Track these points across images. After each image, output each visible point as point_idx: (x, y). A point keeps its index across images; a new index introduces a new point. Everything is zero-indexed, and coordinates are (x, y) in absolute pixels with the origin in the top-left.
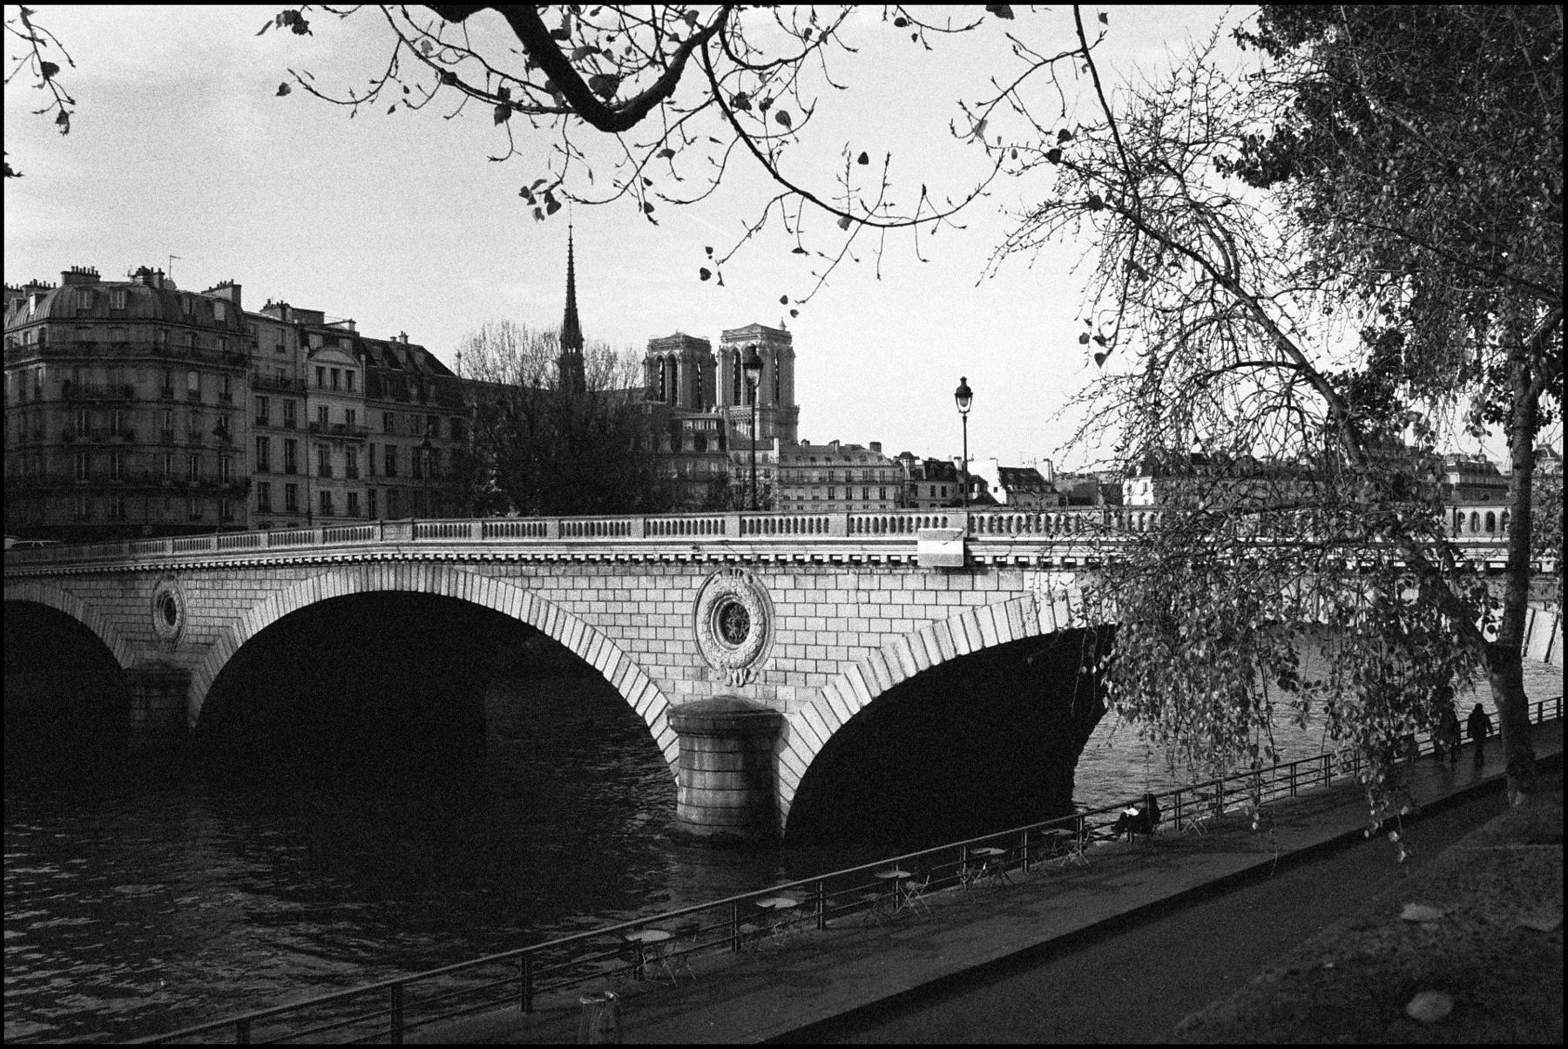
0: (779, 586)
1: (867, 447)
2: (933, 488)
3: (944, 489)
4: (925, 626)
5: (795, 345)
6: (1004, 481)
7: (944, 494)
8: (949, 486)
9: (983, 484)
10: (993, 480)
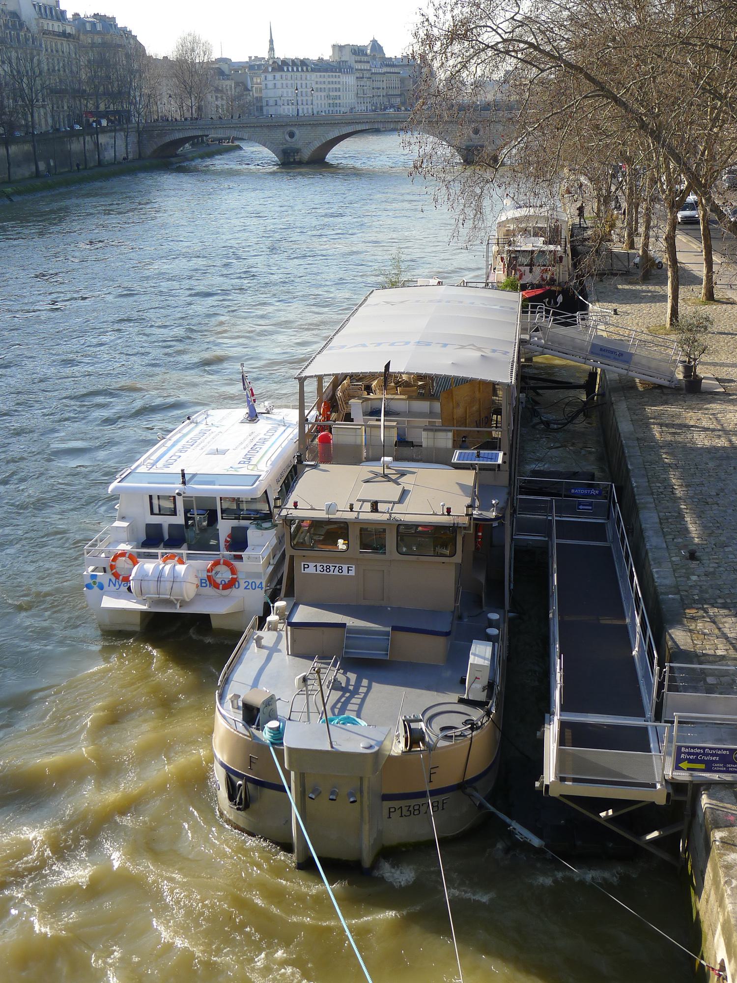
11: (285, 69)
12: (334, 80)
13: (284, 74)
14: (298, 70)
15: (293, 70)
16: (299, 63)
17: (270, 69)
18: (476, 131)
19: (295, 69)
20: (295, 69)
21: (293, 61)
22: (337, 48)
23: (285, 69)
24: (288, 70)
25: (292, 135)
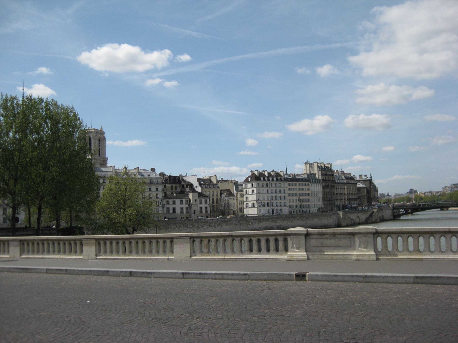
1: (150, 170)
2: (253, 184)
3: (176, 187)
5: (106, 135)
6: (200, 185)
7: (176, 189)
8: (178, 185)
9: (191, 185)
10: (196, 183)
11: (262, 179)
12: (294, 187)
13: (261, 183)
14: (273, 180)
15: (268, 180)
16: (266, 174)
17: (250, 179)
19: (271, 179)
20: (271, 179)
21: (269, 174)
22: (308, 165)
23: (262, 179)
24: (264, 180)
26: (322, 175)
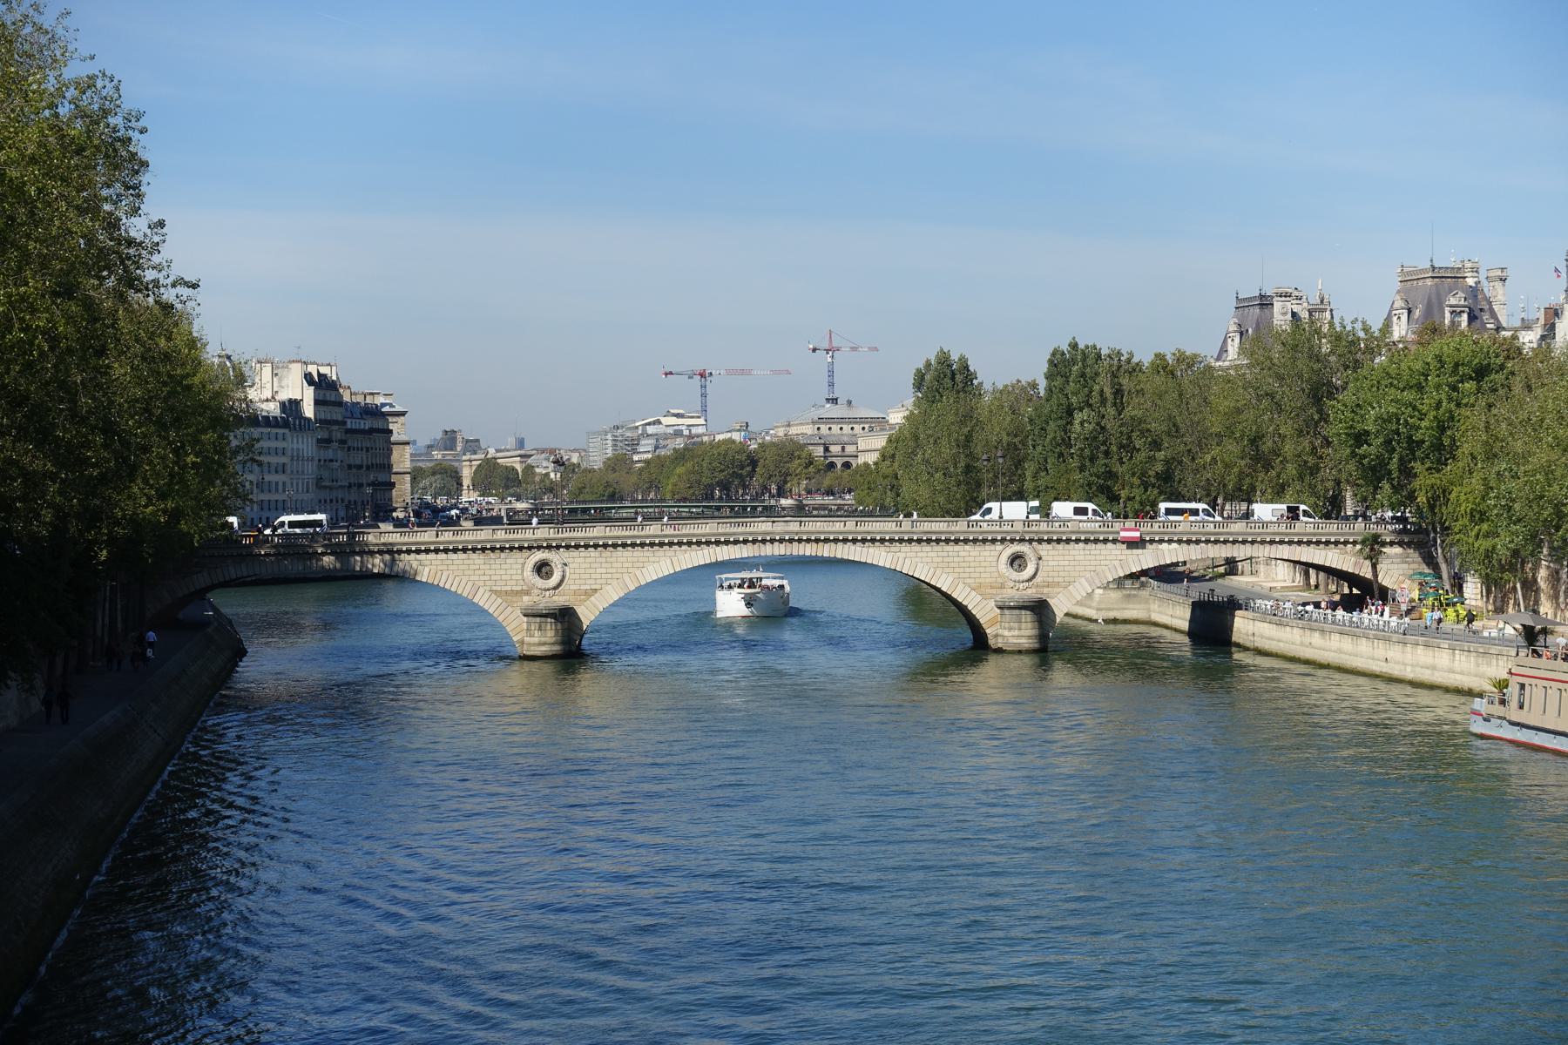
0: (1044, 549)
4: (1117, 563)
18: (542, 569)
25: (542, 569)
26: (317, 402)
